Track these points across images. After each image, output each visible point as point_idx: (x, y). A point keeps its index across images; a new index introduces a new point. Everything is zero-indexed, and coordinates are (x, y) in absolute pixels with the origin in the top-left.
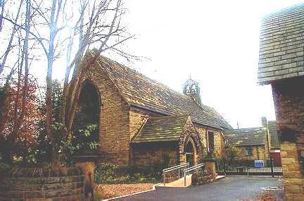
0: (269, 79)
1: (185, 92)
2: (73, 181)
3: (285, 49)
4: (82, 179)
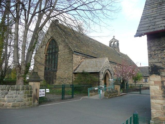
0: (145, 32)
1: (110, 45)
2: (25, 93)
3: (159, 12)
4: (31, 92)
